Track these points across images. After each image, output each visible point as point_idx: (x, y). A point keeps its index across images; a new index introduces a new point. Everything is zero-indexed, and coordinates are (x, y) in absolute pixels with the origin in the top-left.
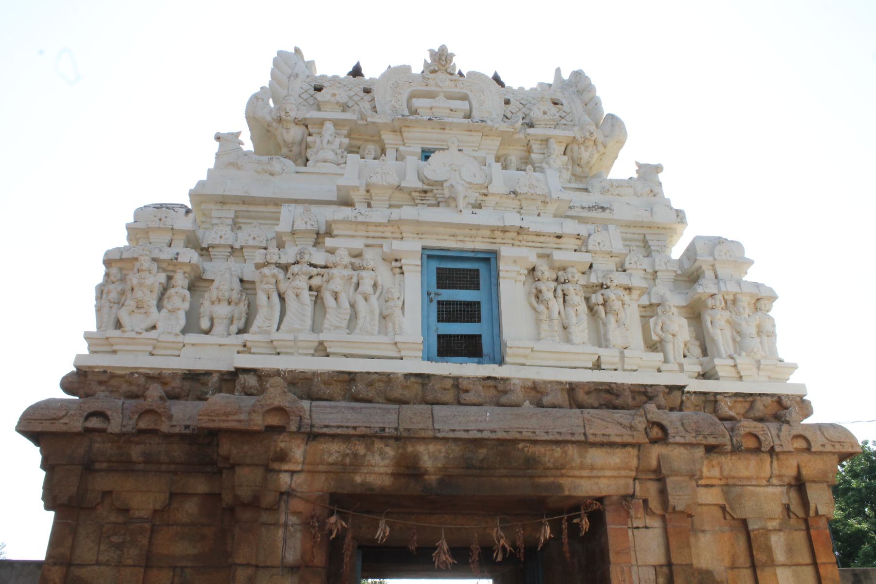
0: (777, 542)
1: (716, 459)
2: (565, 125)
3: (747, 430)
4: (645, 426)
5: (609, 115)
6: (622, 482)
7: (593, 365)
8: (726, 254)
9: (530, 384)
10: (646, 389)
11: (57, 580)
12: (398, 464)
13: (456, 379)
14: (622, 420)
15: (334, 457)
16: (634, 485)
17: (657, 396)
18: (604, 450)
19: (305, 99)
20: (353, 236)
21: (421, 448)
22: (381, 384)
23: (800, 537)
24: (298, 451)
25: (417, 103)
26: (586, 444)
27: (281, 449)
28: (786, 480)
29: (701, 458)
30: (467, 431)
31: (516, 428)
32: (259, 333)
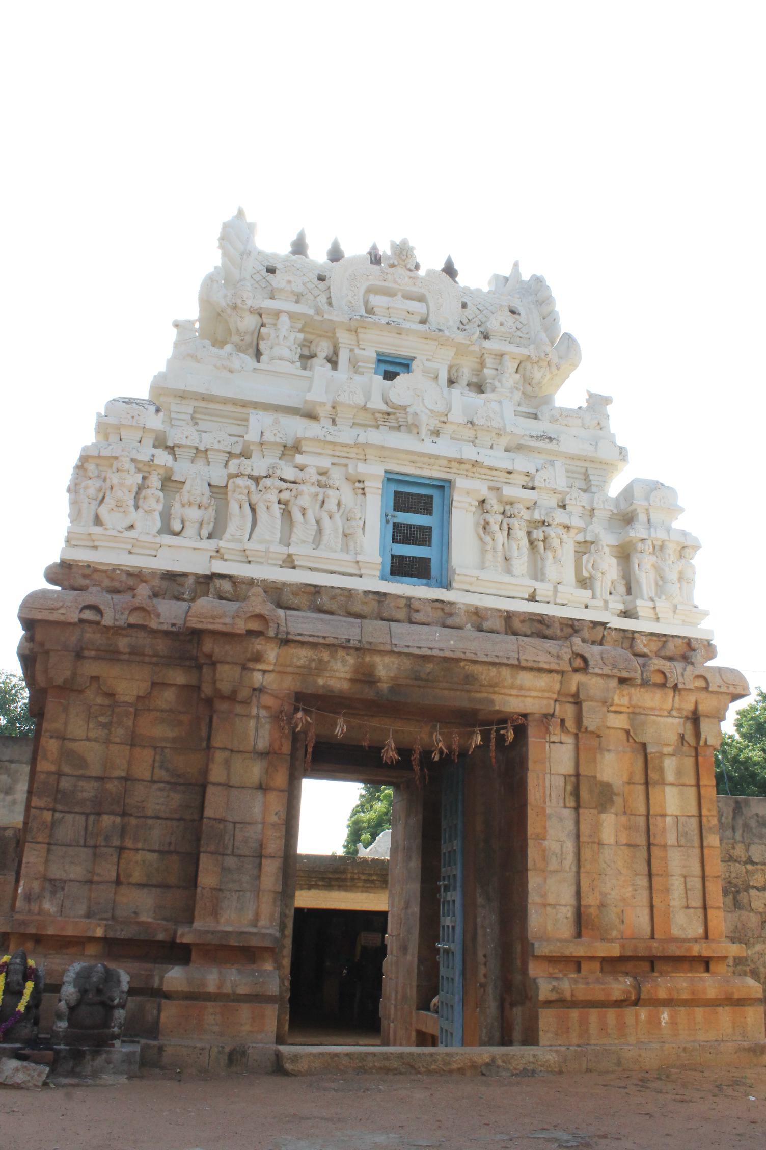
0: (670, 765)
1: (627, 690)
2: (520, 337)
3: (657, 667)
4: (570, 656)
5: (566, 334)
6: (545, 702)
7: (529, 596)
8: (660, 500)
9: (473, 609)
10: (573, 623)
11: (54, 750)
12: (356, 671)
13: (409, 599)
14: (551, 650)
15: (302, 661)
16: (555, 705)
17: (582, 630)
18: (532, 673)
19: (257, 280)
20: (320, 454)
21: (377, 659)
22: (342, 598)
23: (689, 762)
24: (272, 654)
25: (377, 301)
26: (519, 667)
27: (258, 651)
28: (685, 713)
29: (615, 688)
30: (420, 648)
31: (461, 649)
32: (232, 541)
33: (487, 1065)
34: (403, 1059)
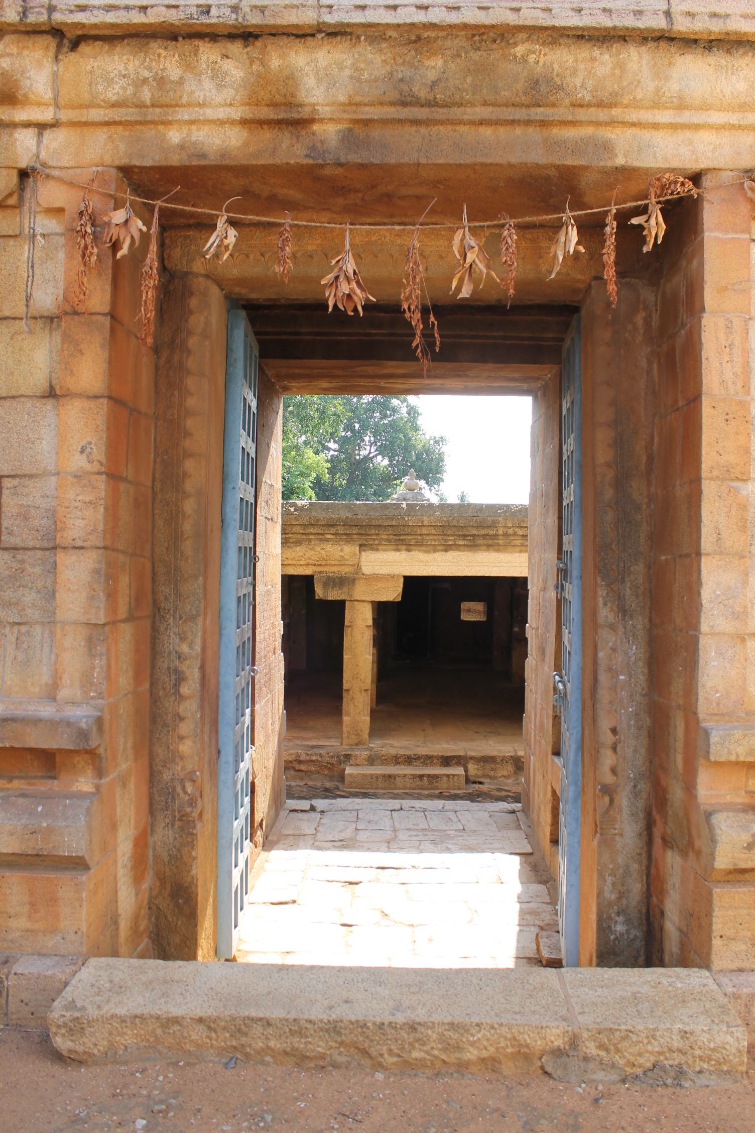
12: (253, 101)
33: (558, 1053)
34: (339, 1034)
